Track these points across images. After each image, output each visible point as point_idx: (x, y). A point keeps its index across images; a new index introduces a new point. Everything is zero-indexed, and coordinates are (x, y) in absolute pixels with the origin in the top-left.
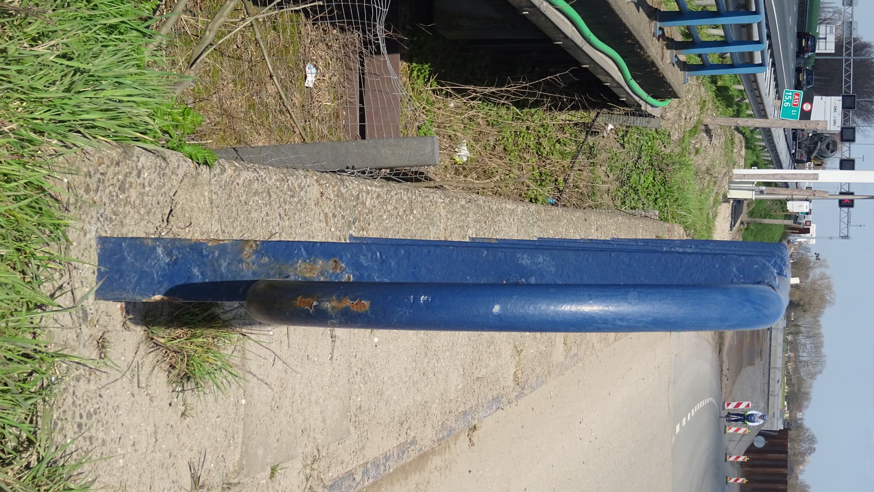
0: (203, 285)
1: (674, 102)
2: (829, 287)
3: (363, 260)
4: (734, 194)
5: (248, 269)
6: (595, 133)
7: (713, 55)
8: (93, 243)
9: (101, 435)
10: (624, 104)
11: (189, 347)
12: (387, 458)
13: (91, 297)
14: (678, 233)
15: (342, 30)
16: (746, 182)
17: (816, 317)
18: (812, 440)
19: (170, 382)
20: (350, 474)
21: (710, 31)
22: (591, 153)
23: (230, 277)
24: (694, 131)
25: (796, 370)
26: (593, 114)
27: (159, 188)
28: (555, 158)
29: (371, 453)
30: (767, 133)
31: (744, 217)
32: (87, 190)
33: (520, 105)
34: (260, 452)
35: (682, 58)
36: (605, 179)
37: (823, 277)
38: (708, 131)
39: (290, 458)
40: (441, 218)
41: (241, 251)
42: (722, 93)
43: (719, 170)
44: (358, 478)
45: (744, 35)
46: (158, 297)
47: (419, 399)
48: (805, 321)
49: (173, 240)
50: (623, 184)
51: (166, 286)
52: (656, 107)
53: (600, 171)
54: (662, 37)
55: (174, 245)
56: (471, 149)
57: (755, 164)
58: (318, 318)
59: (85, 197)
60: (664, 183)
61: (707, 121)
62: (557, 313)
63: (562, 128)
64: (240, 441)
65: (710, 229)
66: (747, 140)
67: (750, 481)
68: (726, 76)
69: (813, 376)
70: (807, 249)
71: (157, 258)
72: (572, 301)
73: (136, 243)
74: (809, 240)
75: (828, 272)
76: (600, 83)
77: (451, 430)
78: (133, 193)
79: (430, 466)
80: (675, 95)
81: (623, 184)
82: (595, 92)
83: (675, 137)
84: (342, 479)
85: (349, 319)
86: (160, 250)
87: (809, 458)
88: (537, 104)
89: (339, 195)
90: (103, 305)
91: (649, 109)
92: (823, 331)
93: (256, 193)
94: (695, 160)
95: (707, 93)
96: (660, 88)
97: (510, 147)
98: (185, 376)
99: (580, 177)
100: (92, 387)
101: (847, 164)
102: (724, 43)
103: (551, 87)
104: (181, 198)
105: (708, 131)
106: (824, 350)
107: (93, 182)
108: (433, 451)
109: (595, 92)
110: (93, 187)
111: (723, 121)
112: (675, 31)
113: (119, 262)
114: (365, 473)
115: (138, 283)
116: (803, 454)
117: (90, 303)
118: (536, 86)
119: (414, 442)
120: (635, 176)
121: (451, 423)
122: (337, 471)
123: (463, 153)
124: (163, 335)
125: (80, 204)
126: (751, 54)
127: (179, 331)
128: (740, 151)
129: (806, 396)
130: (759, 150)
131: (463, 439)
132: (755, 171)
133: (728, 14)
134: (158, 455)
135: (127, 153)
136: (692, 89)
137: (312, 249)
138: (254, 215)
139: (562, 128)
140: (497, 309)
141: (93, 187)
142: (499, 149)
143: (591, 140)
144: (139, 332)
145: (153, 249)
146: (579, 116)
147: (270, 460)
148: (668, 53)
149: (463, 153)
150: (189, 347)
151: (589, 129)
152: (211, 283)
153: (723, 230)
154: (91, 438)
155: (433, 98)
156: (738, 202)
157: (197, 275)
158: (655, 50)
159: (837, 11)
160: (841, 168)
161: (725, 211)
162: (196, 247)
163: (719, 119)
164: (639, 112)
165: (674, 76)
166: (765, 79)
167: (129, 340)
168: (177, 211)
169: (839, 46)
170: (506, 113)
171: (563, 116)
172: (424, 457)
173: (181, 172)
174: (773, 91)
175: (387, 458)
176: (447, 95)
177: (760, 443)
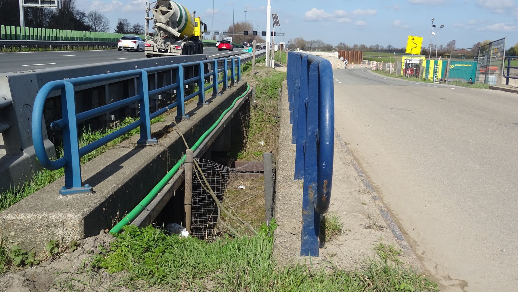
0: (315, 226)
1: (248, 83)
2: (298, 39)
3: (309, 180)
4: (273, 66)
5: (311, 213)
6: (257, 106)
7: (235, 72)
8: (302, 257)
9: (358, 256)
10: (249, 98)
11: (331, 229)
12: (357, 170)
13: (319, 258)
14: (285, 82)
15: (229, 178)
16: (269, 62)
17: (306, 43)
18: (341, 44)
19: (341, 235)
20: (362, 181)
21: (228, 72)
22: (262, 107)
23: (313, 218)
24: (256, 77)
25: (321, 48)
26: (251, 106)
27: (285, 237)
28: (263, 117)
29: (356, 174)
30: (256, 56)
31: (279, 63)
32: (287, 259)
33: (249, 127)
34: (358, 208)
35: (236, 81)
36: (270, 103)
37: (295, 40)
38: (256, 74)
39: (359, 199)
40: (288, 153)
41: (305, 215)
42: (245, 69)
43: (266, 70)
44: (363, 178)
45: (230, 63)
46: (318, 239)
47: (339, 160)
48: (307, 45)
49: (302, 234)
50: (271, 98)
51: (315, 237)
52: (249, 89)
53: (267, 104)
54: (230, 86)
55: (303, 234)
56: (261, 141)
57: (264, 60)
58: (328, 194)
59: (289, 259)
60: (271, 86)
61: (253, 74)
62: (329, 126)
63: (255, 115)
64: (356, 214)
65: (283, 73)
66: (258, 62)
67: (353, 61)
68: (241, 69)
69: (323, 43)
70: (287, 45)
71: (307, 239)
72: (326, 121)
73: (302, 245)
74: (284, 44)
75: (293, 39)
76: (243, 104)
77: (347, 150)
78: (287, 245)
79: (357, 156)
80: (246, 83)
81: (271, 98)
82: (245, 106)
83: (258, 83)
84: (364, 183)
85: (329, 186)
86: (305, 238)
87: (346, 45)
88: (249, 122)
89: (282, 183)
90: (320, 255)
91: (250, 90)
92: (310, 40)
93: (284, 208)
94: (264, 77)
95: (245, 74)
96: (244, 87)
97: (260, 130)
98: (338, 230)
99: (269, 110)
100: (344, 258)
101: (264, 34)
102: (232, 69)
103: (244, 119)
104: (288, 231)
105: (256, 74)
106: (316, 40)
107: (285, 257)
108: (353, 155)
109: (245, 106)
110: (286, 257)
111: (253, 69)
112: (229, 83)
113: (309, 249)
114: (361, 176)
115: (314, 244)
116: (345, 46)
117: (320, 258)
118: (244, 122)
119: (351, 161)
120: (269, 94)
121: (345, 150)
122: (362, 184)
123: (262, 143)
124: (327, 238)
125: (292, 261)
126: (235, 61)
127: (326, 232)
128: (261, 64)
129: (328, 45)
130: (261, 58)
131: (349, 146)
132: (266, 60)
133: (224, 68)
134: (362, 239)
135: (276, 246)
136: (245, 78)
137: (305, 194)
138: (290, 208)
139: (255, 115)
140: (328, 143)
141: (286, 257)
142: (261, 133)
143: (258, 107)
144: (327, 244)
145: (305, 240)
146: (252, 110)
147: (361, 205)
148: (235, 85)
149: (262, 143)
150: (331, 229)
151: (255, 107)
152: (315, 223)
153: (284, 69)
154: (359, 259)
155: (247, 152)
156: (275, 65)
157: (312, 227)
158: (234, 89)
159: (220, 36)
160: (265, 35)
161: (277, 68)
162: (305, 228)
163: (252, 71)
164: (251, 93)
165: (241, 84)
166: (242, 57)
167: (330, 247)
168: (291, 232)
169: (231, 36)
170: (251, 131)
171: (252, 115)
172: (355, 158)
173: (280, 230)
174: (244, 55)
175: (357, 170)
176: (246, 147)
177: (342, 58)
